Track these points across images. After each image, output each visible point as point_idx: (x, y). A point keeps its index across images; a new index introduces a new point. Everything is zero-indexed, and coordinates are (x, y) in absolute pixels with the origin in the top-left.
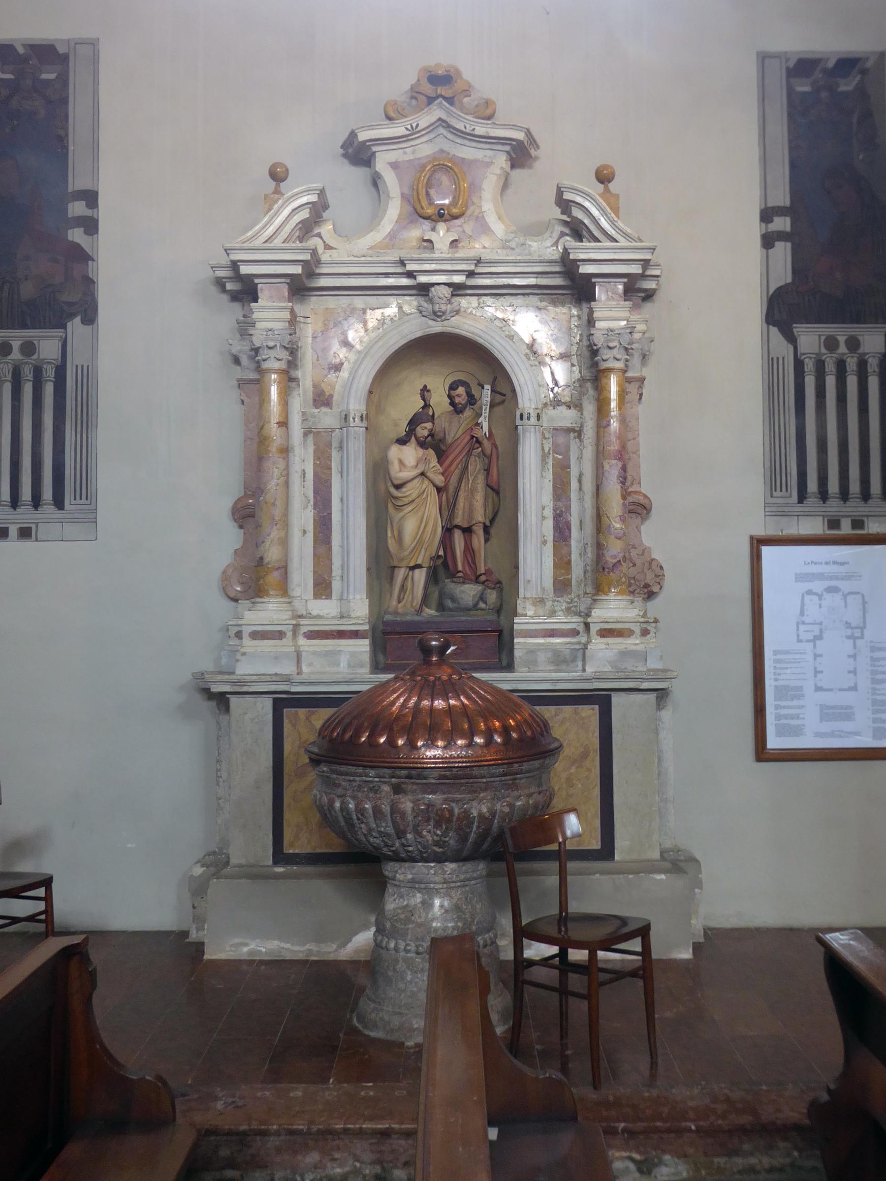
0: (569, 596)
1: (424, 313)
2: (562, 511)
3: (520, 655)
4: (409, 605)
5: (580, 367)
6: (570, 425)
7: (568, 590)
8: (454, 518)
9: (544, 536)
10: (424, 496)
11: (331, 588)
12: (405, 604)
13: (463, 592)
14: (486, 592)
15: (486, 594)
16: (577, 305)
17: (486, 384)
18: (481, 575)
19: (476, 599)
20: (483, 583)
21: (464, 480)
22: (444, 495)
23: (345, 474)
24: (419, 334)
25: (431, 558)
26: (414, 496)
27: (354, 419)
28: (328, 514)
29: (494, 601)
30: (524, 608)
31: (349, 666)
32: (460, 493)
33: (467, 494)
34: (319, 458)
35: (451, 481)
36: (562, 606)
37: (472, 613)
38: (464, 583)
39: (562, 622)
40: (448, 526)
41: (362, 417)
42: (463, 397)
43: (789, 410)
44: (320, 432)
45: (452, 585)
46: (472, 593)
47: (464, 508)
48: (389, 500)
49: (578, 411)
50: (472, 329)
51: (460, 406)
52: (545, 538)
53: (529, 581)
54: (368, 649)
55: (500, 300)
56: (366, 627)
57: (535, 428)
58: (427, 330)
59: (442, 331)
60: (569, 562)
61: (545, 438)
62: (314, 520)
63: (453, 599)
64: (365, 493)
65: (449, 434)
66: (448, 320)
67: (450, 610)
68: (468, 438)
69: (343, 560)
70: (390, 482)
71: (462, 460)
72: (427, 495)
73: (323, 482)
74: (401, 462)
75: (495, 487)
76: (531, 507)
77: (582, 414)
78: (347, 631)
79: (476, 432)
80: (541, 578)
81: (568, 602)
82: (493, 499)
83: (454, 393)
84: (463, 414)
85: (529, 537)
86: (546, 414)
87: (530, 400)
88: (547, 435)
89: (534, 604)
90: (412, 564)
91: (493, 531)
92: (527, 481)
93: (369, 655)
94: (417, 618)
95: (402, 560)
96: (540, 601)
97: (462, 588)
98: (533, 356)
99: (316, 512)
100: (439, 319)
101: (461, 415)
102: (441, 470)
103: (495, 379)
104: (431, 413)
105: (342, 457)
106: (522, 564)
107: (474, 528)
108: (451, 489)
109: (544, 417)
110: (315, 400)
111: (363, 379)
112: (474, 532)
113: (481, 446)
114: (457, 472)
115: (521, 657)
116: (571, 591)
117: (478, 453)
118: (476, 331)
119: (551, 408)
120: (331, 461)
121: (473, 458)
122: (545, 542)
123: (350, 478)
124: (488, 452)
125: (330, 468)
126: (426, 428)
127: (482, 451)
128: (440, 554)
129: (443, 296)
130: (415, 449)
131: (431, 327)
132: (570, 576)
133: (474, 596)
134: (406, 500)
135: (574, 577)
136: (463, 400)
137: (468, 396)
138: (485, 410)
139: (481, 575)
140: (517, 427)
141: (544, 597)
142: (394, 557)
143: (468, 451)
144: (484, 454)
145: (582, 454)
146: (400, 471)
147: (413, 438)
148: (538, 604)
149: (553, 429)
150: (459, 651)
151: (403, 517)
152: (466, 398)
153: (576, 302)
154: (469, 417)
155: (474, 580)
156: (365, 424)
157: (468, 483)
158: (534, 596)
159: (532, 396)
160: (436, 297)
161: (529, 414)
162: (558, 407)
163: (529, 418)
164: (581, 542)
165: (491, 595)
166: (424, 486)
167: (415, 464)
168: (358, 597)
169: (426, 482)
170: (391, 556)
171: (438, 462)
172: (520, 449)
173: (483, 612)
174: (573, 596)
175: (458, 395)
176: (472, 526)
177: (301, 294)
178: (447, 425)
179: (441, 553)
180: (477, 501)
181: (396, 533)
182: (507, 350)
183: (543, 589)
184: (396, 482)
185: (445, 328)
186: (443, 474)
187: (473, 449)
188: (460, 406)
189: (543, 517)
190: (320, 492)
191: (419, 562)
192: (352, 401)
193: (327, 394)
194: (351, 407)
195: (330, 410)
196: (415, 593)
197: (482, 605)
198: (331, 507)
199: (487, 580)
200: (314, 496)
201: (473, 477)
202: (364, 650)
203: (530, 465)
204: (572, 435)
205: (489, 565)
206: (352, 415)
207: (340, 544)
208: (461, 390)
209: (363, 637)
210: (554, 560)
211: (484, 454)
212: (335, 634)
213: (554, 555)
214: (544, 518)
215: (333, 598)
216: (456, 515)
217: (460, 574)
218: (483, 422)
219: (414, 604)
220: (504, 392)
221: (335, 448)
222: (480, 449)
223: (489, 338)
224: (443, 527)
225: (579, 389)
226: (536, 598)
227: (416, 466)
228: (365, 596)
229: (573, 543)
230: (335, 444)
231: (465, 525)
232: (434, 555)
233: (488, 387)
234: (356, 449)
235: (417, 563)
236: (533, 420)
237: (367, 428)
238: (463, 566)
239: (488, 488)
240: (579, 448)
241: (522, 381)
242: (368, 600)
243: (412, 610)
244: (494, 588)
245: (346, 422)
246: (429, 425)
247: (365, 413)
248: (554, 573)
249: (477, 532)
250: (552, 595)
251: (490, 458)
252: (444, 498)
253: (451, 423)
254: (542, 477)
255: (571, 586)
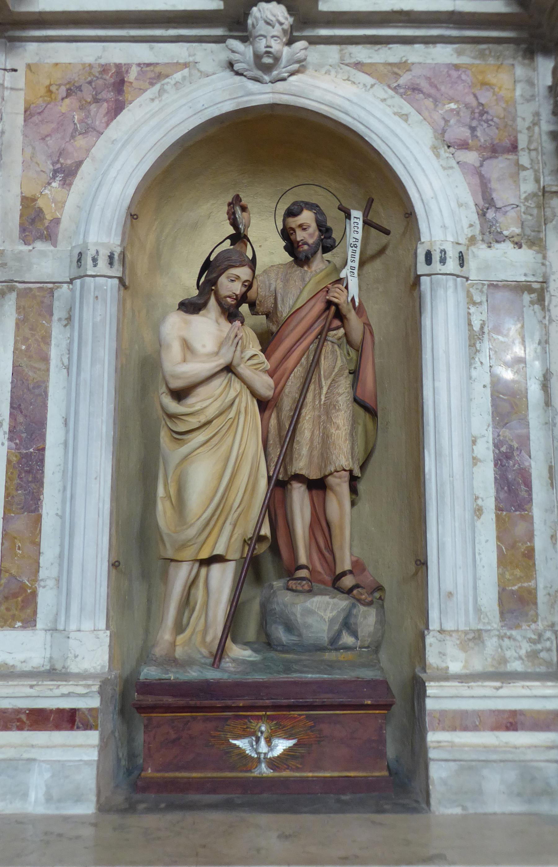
0: (533, 626)
1: (237, 67)
2: (511, 447)
3: (444, 775)
4: (198, 639)
5: (536, 172)
6: (523, 279)
7: (532, 613)
8: (291, 459)
9: (477, 498)
10: (232, 414)
11: (36, 604)
12: (190, 639)
13: (309, 612)
14: (355, 611)
15: (356, 616)
16: (526, 61)
17: (355, 209)
18: (344, 574)
19: (337, 627)
20: (349, 591)
21: (312, 387)
22: (274, 415)
23: (74, 369)
24: (228, 107)
25: (245, 541)
26: (210, 413)
27: (95, 260)
28: (39, 450)
29: (372, 629)
30: (442, 654)
31: (49, 799)
32: (304, 411)
33: (317, 413)
34: (25, 340)
35: (287, 390)
36: (520, 647)
37: (329, 656)
38: (310, 592)
39: (536, 697)
40: (281, 477)
41: (111, 257)
42: (311, 230)
43: (200, 517)
44: (30, 289)
45: (288, 597)
46: (329, 615)
47: (312, 440)
48: (163, 422)
49: (538, 252)
50: (329, 98)
51: (306, 247)
52: (480, 502)
53: (450, 595)
54: (94, 755)
55: (381, 51)
56: (95, 703)
57: (456, 280)
58: (245, 99)
59: (272, 101)
60: (530, 554)
61: (474, 303)
62: (9, 462)
63: (290, 627)
64: (112, 406)
65: (283, 300)
66: (284, 79)
67: (285, 649)
68: (320, 306)
69: (62, 545)
70: (164, 386)
71: (308, 348)
72: (238, 413)
73: (31, 386)
74: (187, 346)
75: (369, 401)
76: (451, 438)
77: (544, 257)
78: (51, 711)
79: (336, 295)
80: (475, 588)
81: (530, 641)
82: (365, 426)
83: (293, 222)
84: (309, 267)
85: (448, 500)
86: (474, 256)
87: (444, 227)
88: (477, 298)
89: (463, 646)
90: (204, 555)
91: (361, 487)
92: (441, 384)
93: (95, 772)
94: (212, 675)
95: (183, 546)
96: (474, 638)
97: (308, 604)
98: (445, 152)
99: (13, 446)
100: (267, 78)
101: (306, 268)
102: (267, 365)
103: (371, 201)
104: (250, 255)
105: (71, 338)
106: (435, 561)
107: (331, 480)
108: (287, 404)
109: (472, 264)
110: (23, 229)
111: (117, 188)
112: (332, 490)
113: (343, 326)
114: (299, 371)
115: (444, 782)
116: (537, 615)
117: (339, 339)
118: (338, 101)
119: (484, 246)
120: (48, 344)
121: (328, 347)
122: (478, 511)
123: (83, 375)
124: (357, 335)
125: (46, 359)
126: (238, 278)
127: (346, 334)
128: (262, 533)
129: (273, 19)
130: (217, 322)
131: (252, 94)
132: (532, 584)
133: (332, 621)
134: (194, 422)
135: (541, 586)
136: (311, 235)
137: (320, 231)
138: (353, 256)
139: (344, 574)
140: (418, 277)
141: (480, 627)
142: (165, 538)
143: (320, 333)
144: (349, 342)
145: (547, 334)
146: (185, 360)
147: (212, 301)
148: (471, 644)
149: (489, 286)
150: (302, 750)
151: (186, 458)
152: (317, 233)
153: (524, 57)
154: (321, 271)
155: (330, 583)
156: (117, 271)
157: (320, 394)
158: (462, 627)
159: (448, 222)
160: (261, 23)
161: (443, 252)
162: (497, 245)
163: (443, 261)
164: (552, 512)
165: (365, 618)
166: (232, 394)
167: (216, 349)
168: (87, 625)
169: (237, 385)
170: (161, 537)
171: (263, 351)
172: (426, 321)
173: (349, 655)
174: (540, 625)
175: (301, 226)
176: (326, 476)
177: (10, 33)
178: (280, 285)
179: (266, 531)
180: (338, 428)
181: (173, 491)
182: (397, 135)
183: (478, 610)
184: (176, 384)
185: (277, 96)
186: (271, 374)
187: (330, 330)
188: (306, 247)
189: (474, 458)
190: (23, 406)
191: (219, 550)
192: (94, 228)
193: (49, 217)
194: (92, 238)
195: (52, 248)
196: (211, 614)
197: (347, 639)
198: (43, 437)
199: (357, 586)
200: (11, 414)
201: (329, 382)
202: (86, 758)
203: (447, 353)
204: (527, 298)
205: (357, 552)
206: (91, 252)
207: (59, 513)
208: (307, 217)
209: (87, 726)
210: (499, 547)
211: (349, 342)
212: (24, 717)
213: (499, 538)
214: (475, 461)
215: (39, 625)
216: (295, 455)
217: (303, 573)
218: (350, 278)
219: (209, 639)
220: (386, 226)
221: (60, 320)
222: (342, 331)
223: (363, 114)
224: (270, 478)
225: (535, 212)
226: (466, 633)
227: (217, 353)
228: (102, 624)
229: (537, 512)
230: (59, 313)
231: (314, 475)
232: (250, 536)
233: (357, 214)
234: (98, 319)
235: (215, 553)
236: (452, 265)
237: (121, 280)
238: (310, 557)
239: (357, 407)
240: (541, 322)
241: (428, 193)
242: (108, 632)
243: (205, 651)
244: (370, 604)
245: (79, 267)
246: (244, 273)
247: (118, 250)
248: (501, 576)
249: (338, 489)
250: (495, 622)
251: (360, 350)
252: (273, 422)
253: (288, 281)
254: (470, 378)
255: (536, 604)
